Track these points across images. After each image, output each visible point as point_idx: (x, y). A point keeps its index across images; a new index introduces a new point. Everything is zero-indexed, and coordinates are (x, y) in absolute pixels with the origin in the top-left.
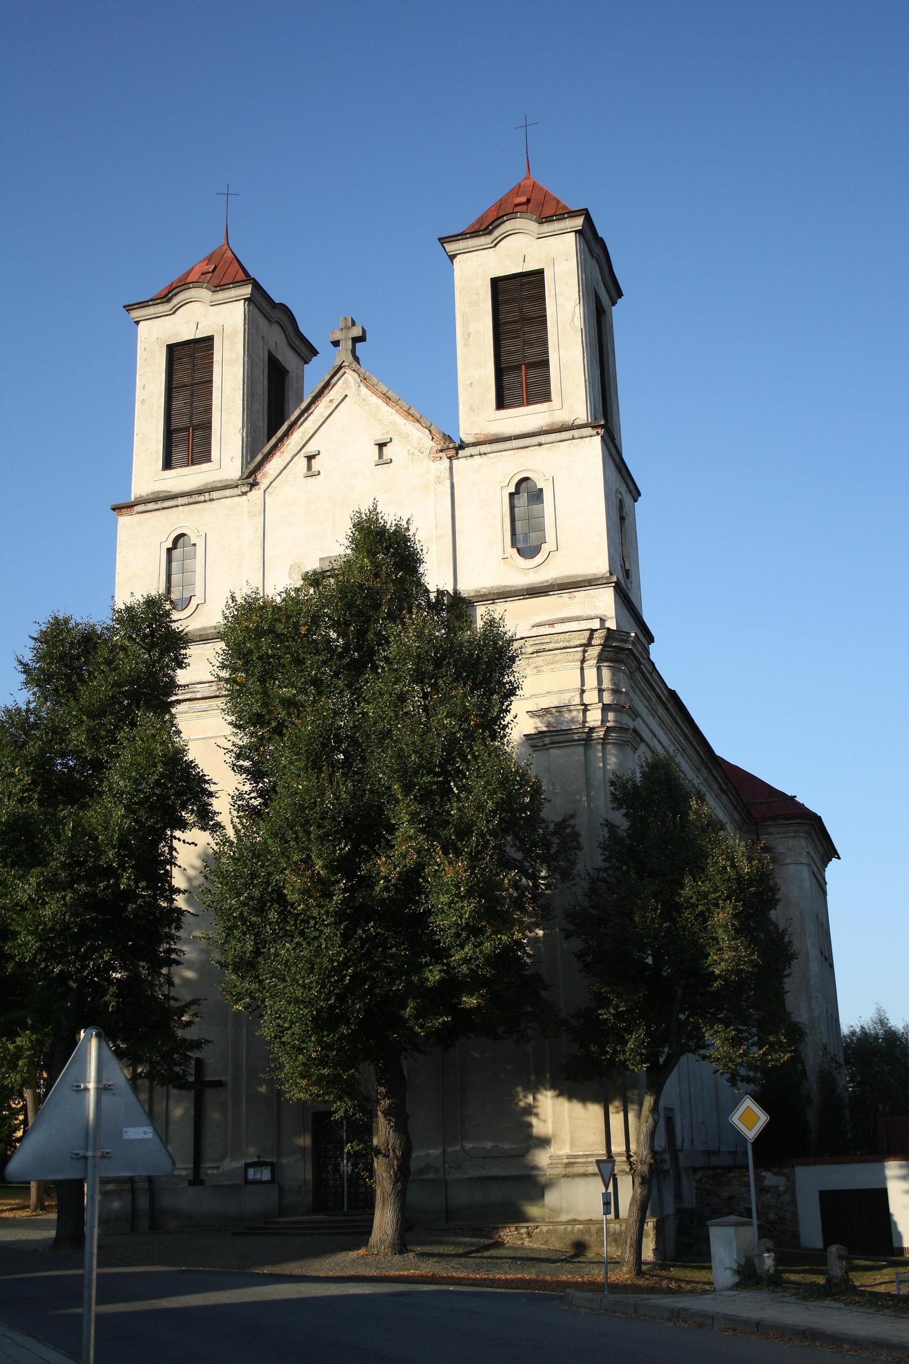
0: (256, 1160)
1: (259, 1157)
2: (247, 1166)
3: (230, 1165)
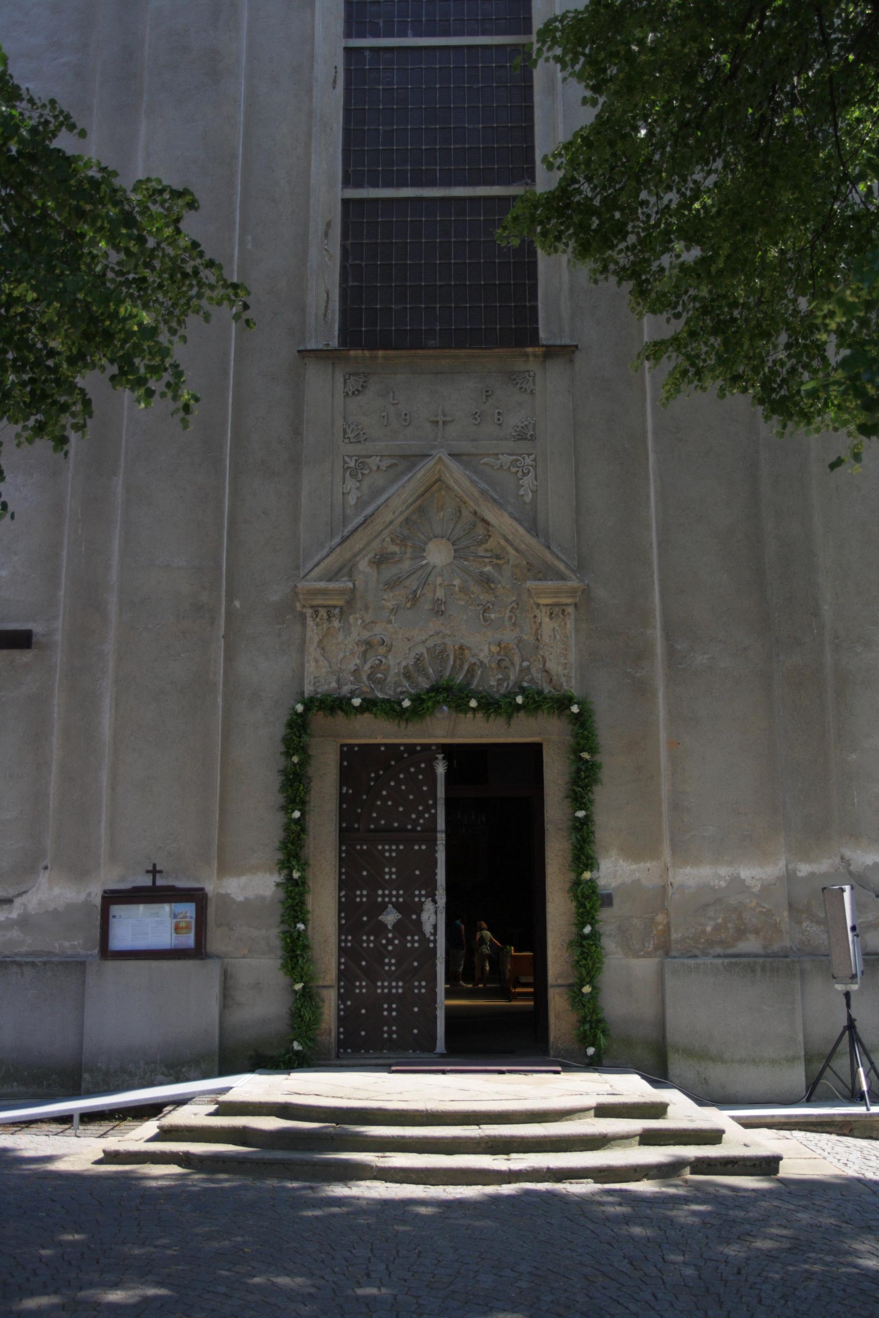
0: (146, 881)
1: (154, 872)
2: (113, 898)
3: (53, 893)
